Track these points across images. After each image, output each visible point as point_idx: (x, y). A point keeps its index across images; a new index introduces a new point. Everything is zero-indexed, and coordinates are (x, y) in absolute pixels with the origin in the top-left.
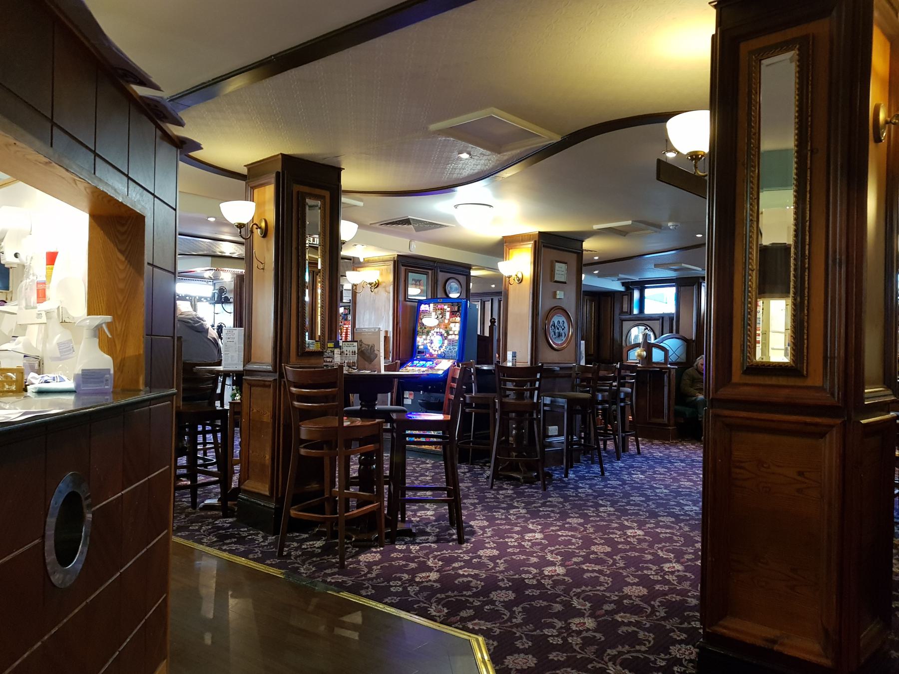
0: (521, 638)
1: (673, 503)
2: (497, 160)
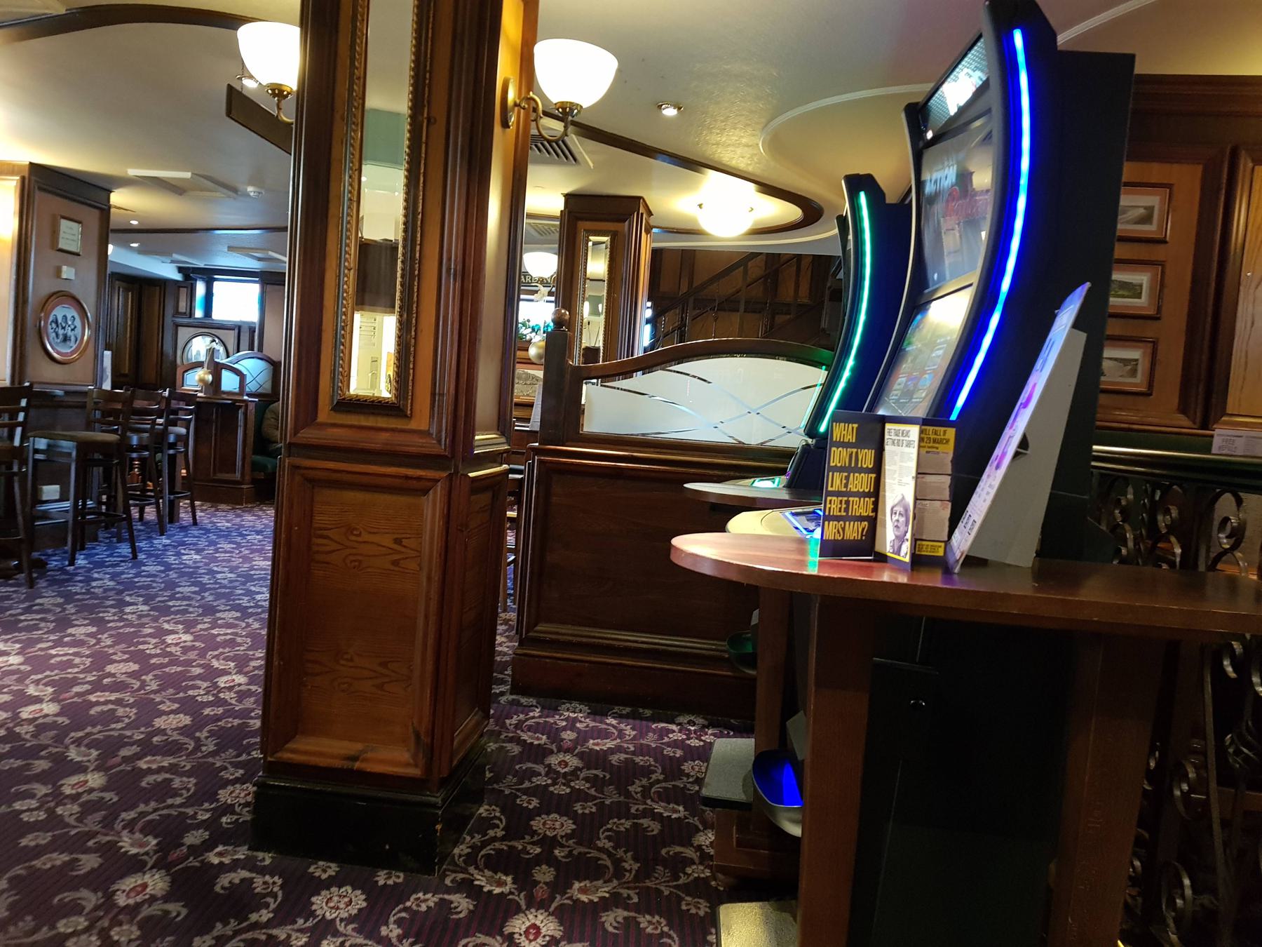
1: (241, 592)
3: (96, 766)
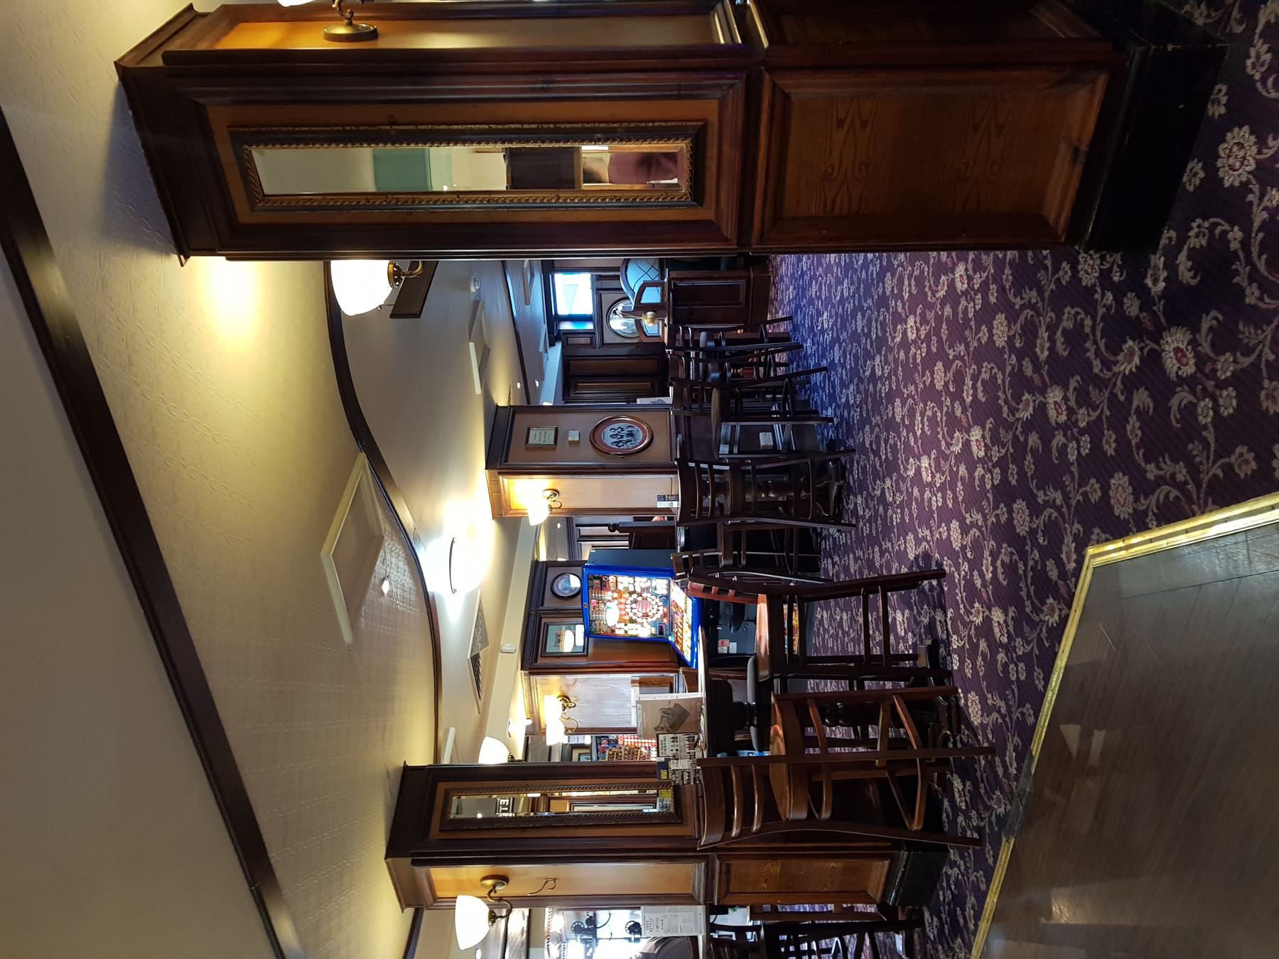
0: (1085, 494)
1: (864, 274)
2: (392, 540)
3: (1040, 395)
